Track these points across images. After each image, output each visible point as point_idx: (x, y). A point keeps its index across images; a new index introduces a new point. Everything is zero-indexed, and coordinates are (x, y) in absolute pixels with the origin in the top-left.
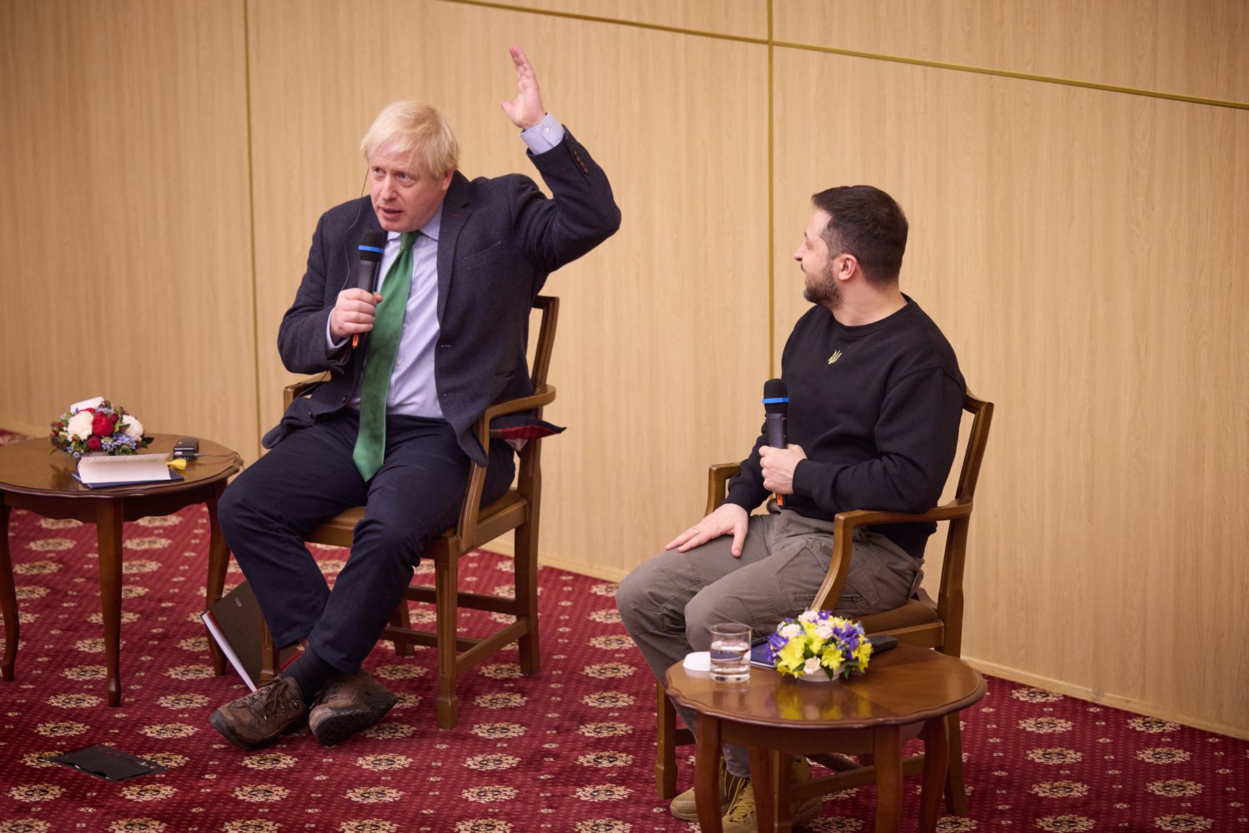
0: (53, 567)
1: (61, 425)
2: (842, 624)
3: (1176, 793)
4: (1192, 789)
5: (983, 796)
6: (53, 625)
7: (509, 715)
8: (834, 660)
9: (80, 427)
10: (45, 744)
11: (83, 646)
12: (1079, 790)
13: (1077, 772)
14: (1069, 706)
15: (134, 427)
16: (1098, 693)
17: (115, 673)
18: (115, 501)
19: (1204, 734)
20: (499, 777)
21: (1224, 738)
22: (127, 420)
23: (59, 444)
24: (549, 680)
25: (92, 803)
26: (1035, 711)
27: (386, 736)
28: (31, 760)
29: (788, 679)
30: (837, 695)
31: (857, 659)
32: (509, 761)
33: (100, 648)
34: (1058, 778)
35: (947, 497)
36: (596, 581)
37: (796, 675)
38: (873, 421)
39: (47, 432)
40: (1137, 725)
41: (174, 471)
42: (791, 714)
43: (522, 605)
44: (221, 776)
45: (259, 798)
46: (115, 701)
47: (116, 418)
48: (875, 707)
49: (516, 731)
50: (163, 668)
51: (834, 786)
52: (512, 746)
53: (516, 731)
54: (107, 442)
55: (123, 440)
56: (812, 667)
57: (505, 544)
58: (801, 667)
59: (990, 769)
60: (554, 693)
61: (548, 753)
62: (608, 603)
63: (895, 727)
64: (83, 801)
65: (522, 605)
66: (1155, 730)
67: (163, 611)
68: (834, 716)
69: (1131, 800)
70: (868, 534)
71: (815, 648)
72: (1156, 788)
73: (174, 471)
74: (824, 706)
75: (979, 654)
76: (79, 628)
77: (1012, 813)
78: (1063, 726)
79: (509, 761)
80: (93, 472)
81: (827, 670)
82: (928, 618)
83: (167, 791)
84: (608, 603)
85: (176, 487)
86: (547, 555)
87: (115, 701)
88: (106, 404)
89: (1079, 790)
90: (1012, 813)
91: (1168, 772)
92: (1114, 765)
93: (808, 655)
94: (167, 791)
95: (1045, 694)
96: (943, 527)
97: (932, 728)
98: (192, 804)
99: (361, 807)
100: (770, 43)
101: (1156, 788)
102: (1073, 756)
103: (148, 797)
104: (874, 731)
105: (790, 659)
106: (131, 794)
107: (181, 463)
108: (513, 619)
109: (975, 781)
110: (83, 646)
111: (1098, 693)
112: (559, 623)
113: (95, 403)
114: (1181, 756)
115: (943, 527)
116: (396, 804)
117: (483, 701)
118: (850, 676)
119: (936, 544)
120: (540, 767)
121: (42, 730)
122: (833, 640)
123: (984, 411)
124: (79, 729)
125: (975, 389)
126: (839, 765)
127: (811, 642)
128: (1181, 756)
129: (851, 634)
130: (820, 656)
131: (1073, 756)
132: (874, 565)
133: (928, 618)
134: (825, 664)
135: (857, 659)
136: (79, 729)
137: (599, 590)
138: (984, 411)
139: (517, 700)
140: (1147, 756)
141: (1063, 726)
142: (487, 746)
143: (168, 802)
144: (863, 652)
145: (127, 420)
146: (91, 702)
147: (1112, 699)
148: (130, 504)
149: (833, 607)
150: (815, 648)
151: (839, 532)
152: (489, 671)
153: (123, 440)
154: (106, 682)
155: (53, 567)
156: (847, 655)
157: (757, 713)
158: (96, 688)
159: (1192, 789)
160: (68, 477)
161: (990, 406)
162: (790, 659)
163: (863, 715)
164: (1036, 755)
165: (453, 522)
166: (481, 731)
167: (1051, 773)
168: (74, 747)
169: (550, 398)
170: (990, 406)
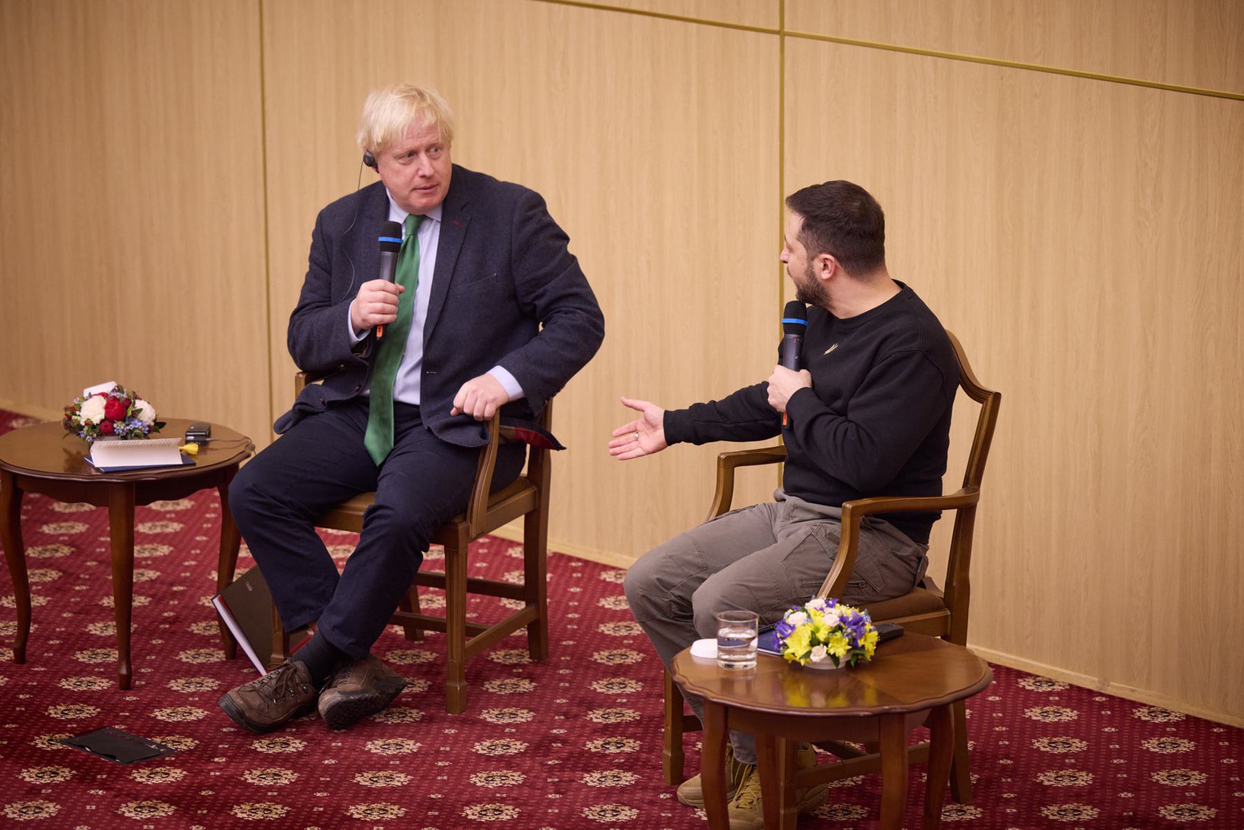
0: (66, 551)
1: (74, 410)
2: (849, 612)
3: (1180, 783)
4: (1197, 778)
6: (64, 608)
7: (517, 700)
8: (840, 648)
9: (93, 411)
10: (56, 726)
12: (1084, 779)
13: (1082, 761)
14: (1076, 696)
16: (1105, 682)
17: (126, 656)
19: (1209, 724)
20: (507, 762)
22: (139, 404)
24: (557, 667)
25: (102, 785)
26: (1041, 699)
28: (41, 743)
29: (795, 666)
30: (843, 682)
31: (863, 647)
33: (111, 632)
34: (1063, 766)
35: (952, 483)
36: (605, 568)
37: (803, 662)
38: (872, 413)
39: (60, 416)
40: (1142, 714)
41: (186, 456)
42: (797, 701)
43: (532, 591)
44: (231, 759)
45: (268, 782)
46: (126, 684)
47: (128, 402)
48: (881, 695)
49: (524, 716)
51: (841, 773)
52: (520, 732)
53: (524, 716)
54: (119, 426)
55: (136, 424)
56: (819, 655)
57: (514, 530)
58: (808, 654)
61: (556, 738)
62: (616, 589)
63: (901, 715)
64: (93, 783)
65: (532, 591)
66: (1160, 719)
67: (175, 595)
68: (840, 704)
69: (1136, 789)
71: (822, 636)
74: (830, 694)
75: (985, 644)
76: (91, 611)
78: (1069, 715)
79: (517, 747)
80: (104, 456)
81: (834, 657)
82: (938, 609)
83: (177, 774)
84: (616, 589)
85: (188, 471)
86: (555, 544)
87: (126, 684)
88: (119, 389)
89: (1084, 779)
90: (1017, 802)
92: (1119, 754)
93: (814, 642)
94: (177, 774)
95: (1050, 682)
96: (949, 517)
97: (938, 716)
98: (201, 788)
99: (369, 791)
100: (781, 33)
102: (1078, 745)
103: (157, 780)
104: (880, 719)
105: (796, 647)
106: (141, 776)
107: (193, 448)
108: (522, 605)
110: (95, 629)
111: (1105, 682)
113: (108, 387)
114: (1186, 746)
116: (404, 788)
117: (492, 686)
118: (856, 663)
119: (943, 530)
120: (548, 752)
122: (839, 628)
123: (990, 401)
124: (90, 711)
127: (817, 630)
128: (1186, 746)
129: (858, 622)
130: (826, 644)
131: (1078, 745)
134: (832, 652)
135: (863, 647)
136: (90, 711)
137: (608, 577)
140: (1152, 745)
141: (1069, 715)
142: (496, 731)
143: (178, 785)
144: (870, 641)
145: (139, 404)
146: (102, 684)
147: (1118, 688)
149: (839, 595)
152: (498, 656)
153: (136, 424)
154: (117, 665)
155: (66, 551)
156: (853, 643)
157: (763, 700)
158: (106, 671)
159: (1197, 778)
160: (80, 461)
161: (997, 396)
162: (796, 647)
163: (869, 704)
164: (1042, 744)
165: (462, 508)
166: (490, 716)
167: (1056, 762)
168: (84, 729)
170: (997, 396)
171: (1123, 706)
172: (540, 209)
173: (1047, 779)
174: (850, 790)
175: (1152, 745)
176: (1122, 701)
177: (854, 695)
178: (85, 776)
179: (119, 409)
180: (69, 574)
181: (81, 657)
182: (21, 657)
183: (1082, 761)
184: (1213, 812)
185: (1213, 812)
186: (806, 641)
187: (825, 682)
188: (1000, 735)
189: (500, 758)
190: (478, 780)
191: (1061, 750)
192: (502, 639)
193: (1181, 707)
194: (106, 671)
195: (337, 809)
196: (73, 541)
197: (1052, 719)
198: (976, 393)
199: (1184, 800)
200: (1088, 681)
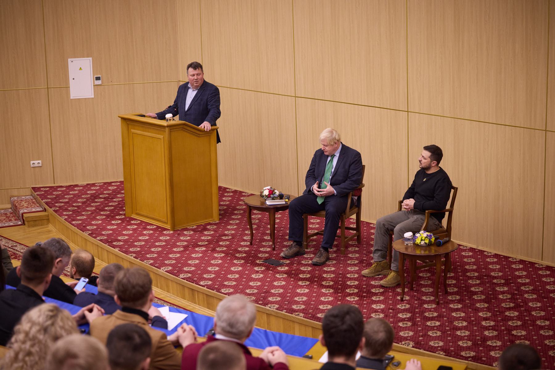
0: (257, 221)
1: (262, 192)
2: (428, 234)
3: (495, 268)
4: (498, 267)
5: (455, 268)
6: (259, 233)
7: (355, 252)
8: (427, 241)
9: (266, 193)
10: (260, 258)
11: (246, 232)
12: (475, 267)
13: (474, 264)
14: (496, 256)
15: (277, 193)
16: (478, 247)
17: (274, 243)
18: (274, 208)
19: (525, 261)
20: (355, 265)
21: (529, 262)
22: (276, 191)
23: (262, 196)
24: (363, 245)
25: (271, 270)
26: (465, 251)
27: (309, 250)
28: (258, 262)
29: (418, 245)
30: (428, 248)
32: (356, 262)
33: (269, 238)
34: (470, 265)
35: (448, 207)
36: (371, 224)
38: (432, 192)
39: (260, 194)
40: (486, 253)
41: (286, 201)
42: (418, 252)
43: (358, 229)
44: (297, 265)
45: (306, 269)
46: (274, 249)
47: (273, 191)
48: (435, 251)
49: (357, 255)
50: (283, 242)
51: (425, 267)
52: (357, 259)
53: (357, 255)
54: (272, 196)
55: (275, 195)
56: (423, 243)
57: (354, 217)
59: (456, 263)
60: (364, 247)
61: (364, 260)
62: (374, 228)
63: (440, 255)
64: (269, 270)
65: (358, 229)
66: (490, 254)
67: (281, 230)
68: (427, 253)
69: (486, 269)
70: (432, 215)
71: (423, 239)
72: (490, 266)
73: (286, 201)
74: (425, 251)
75: (456, 239)
76: (264, 234)
77: (461, 272)
78: (471, 254)
79: (356, 262)
80: (269, 202)
81: (426, 243)
82: (445, 232)
83: (287, 268)
84: (374, 228)
85: (286, 205)
86: (362, 219)
87: (274, 249)
88: (271, 188)
89: (475, 267)
90: (461, 272)
91: (493, 263)
92: (482, 262)
93: (422, 240)
94: (287, 268)
95: (466, 247)
96: (447, 214)
97: (447, 255)
98: (292, 271)
99: (327, 271)
100: (408, 112)
101: (490, 266)
102: (473, 260)
103: (283, 269)
104: (436, 256)
105: (418, 241)
106: (279, 268)
107: (287, 200)
108: (355, 232)
109: (453, 265)
110: (266, 238)
111: (478, 247)
112: (364, 233)
113: (269, 187)
114: (495, 260)
115: (447, 214)
116: (334, 271)
117: (350, 249)
118: (430, 245)
120: (363, 263)
121: (259, 255)
123: (456, 189)
124: (267, 255)
125: (454, 184)
126: (426, 263)
128: (495, 260)
129: (430, 236)
131: (473, 260)
132: (435, 221)
133: (444, 232)
136: (267, 255)
137: (372, 225)
138: (456, 189)
139: (357, 249)
140: (488, 260)
141: (471, 254)
142: (352, 259)
143: (287, 270)
144: (433, 239)
145: (276, 191)
146: (269, 249)
147: (480, 248)
148: (277, 209)
149: (426, 230)
150: (423, 239)
151: (426, 214)
152: (350, 243)
153: (275, 195)
154: (272, 245)
155: (257, 221)
156: (430, 240)
157: (410, 252)
158: (269, 246)
159: (498, 267)
160: (263, 203)
162: (418, 241)
163: (433, 253)
164: (465, 260)
165: (344, 211)
166: (350, 255)
167: (469, 264)
168: (266, 259)
169: (364, 186)
171: (482, 252)
172: (217, 96)
173: (467, 267)
174: (427, 270)
175: (488, 260)
176: (481, 251)
177: (430, 251)
178: (268, 269)
179: (271, 192)
180: (259, 227)
181: (264, 244)
182: (251, 244)
183: (474, 264)
184: (502, 274)
185: (502, 274)
186: (420, 240)
187: (424, 248)
188: (482, 265)
189: (353, 264)
190: (349, 269)
191: (470, 261)
192: (352, 239)
193: (494, 252)
194: (269, 246)
195: (321, 275)
196: (259, 219)
197: (467, 254)
198: (454, 188)
199: (496, 271)
200: (474, 246)
